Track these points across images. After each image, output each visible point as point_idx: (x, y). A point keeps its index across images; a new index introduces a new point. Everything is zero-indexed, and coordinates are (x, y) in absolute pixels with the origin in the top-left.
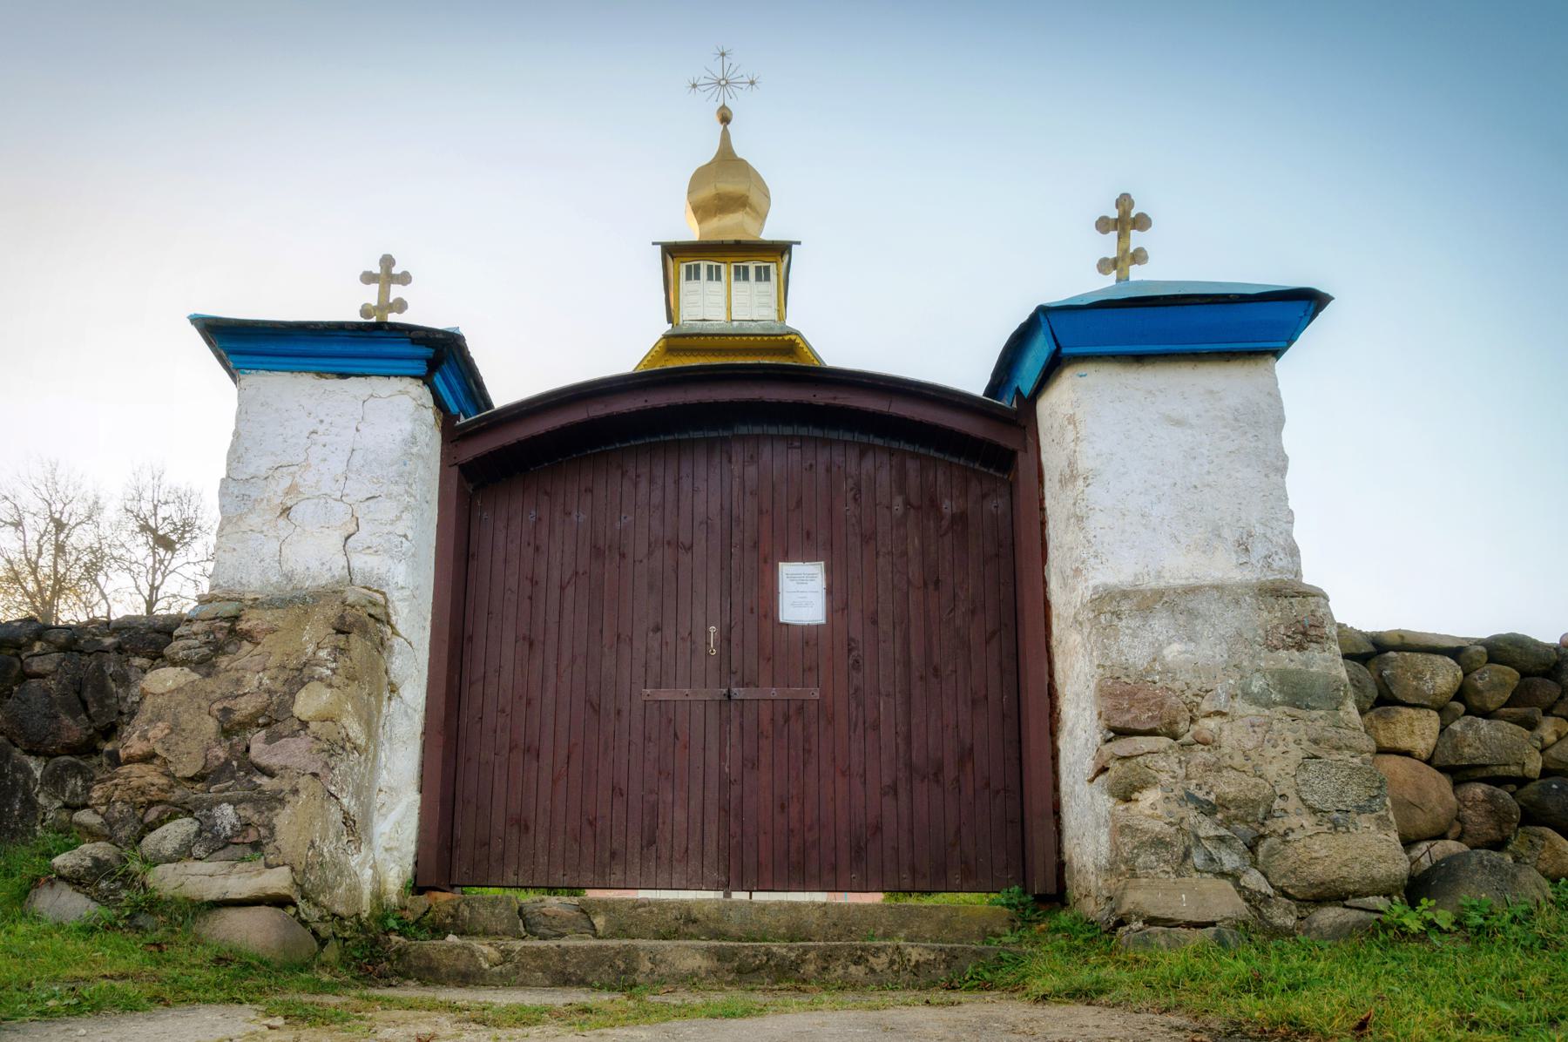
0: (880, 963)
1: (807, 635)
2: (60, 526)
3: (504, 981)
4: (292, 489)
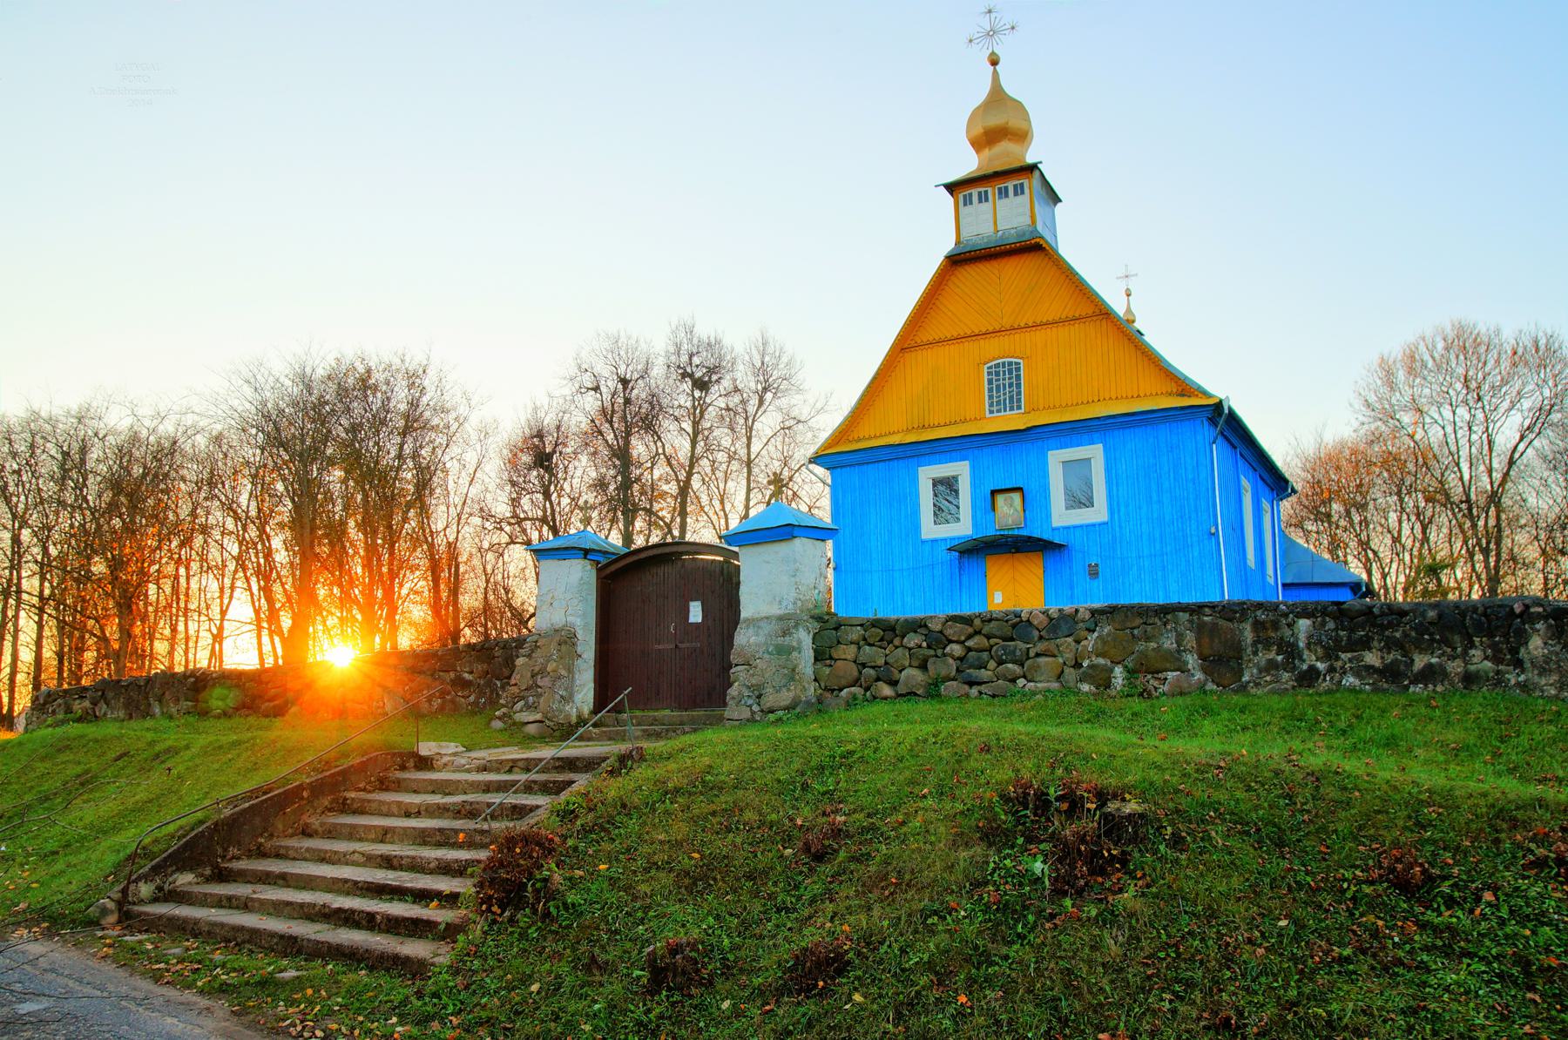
1: (697, 624)
2: (624, 382)
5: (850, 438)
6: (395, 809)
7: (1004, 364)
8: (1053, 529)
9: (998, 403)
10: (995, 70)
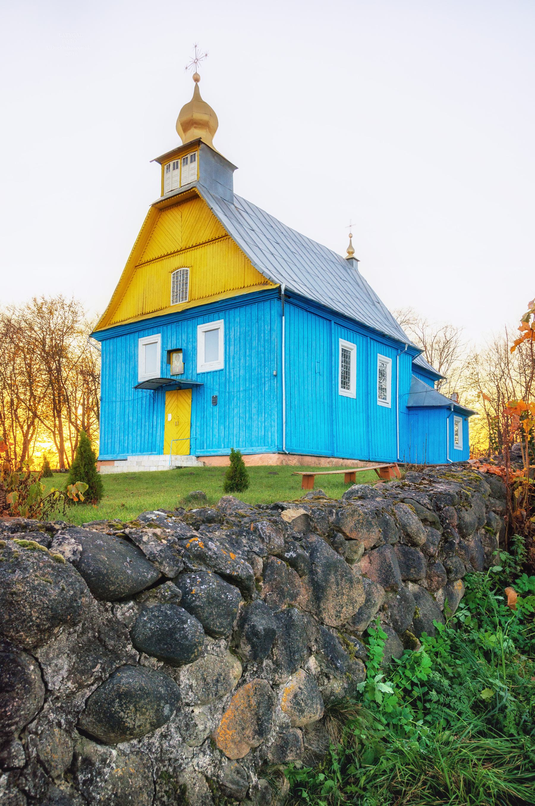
10: (197, 84)
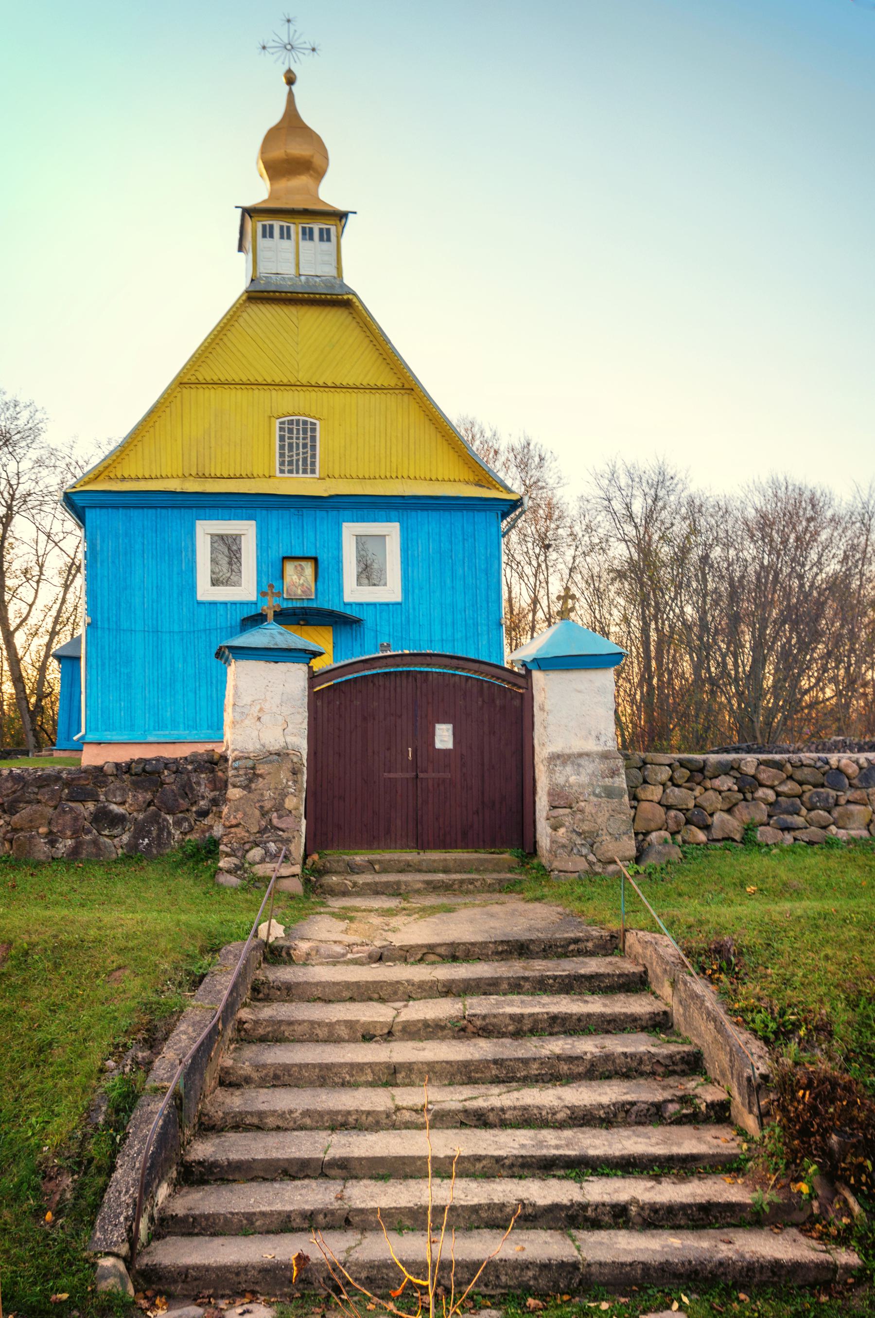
0: (478, 884)
1: (445, 752)
3: (358, 894)
4: (261, 710)
5: (112, 476)
6: (343, 1032)
7: (298, 421)
8: (345, 604)
9: (290, 463)
